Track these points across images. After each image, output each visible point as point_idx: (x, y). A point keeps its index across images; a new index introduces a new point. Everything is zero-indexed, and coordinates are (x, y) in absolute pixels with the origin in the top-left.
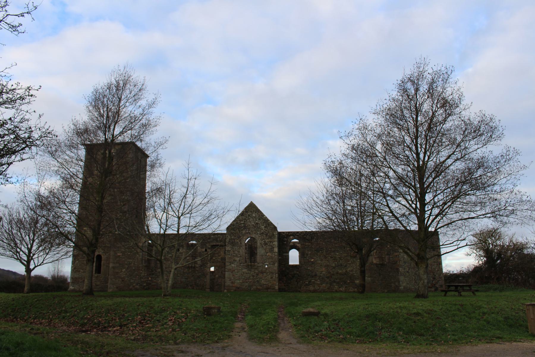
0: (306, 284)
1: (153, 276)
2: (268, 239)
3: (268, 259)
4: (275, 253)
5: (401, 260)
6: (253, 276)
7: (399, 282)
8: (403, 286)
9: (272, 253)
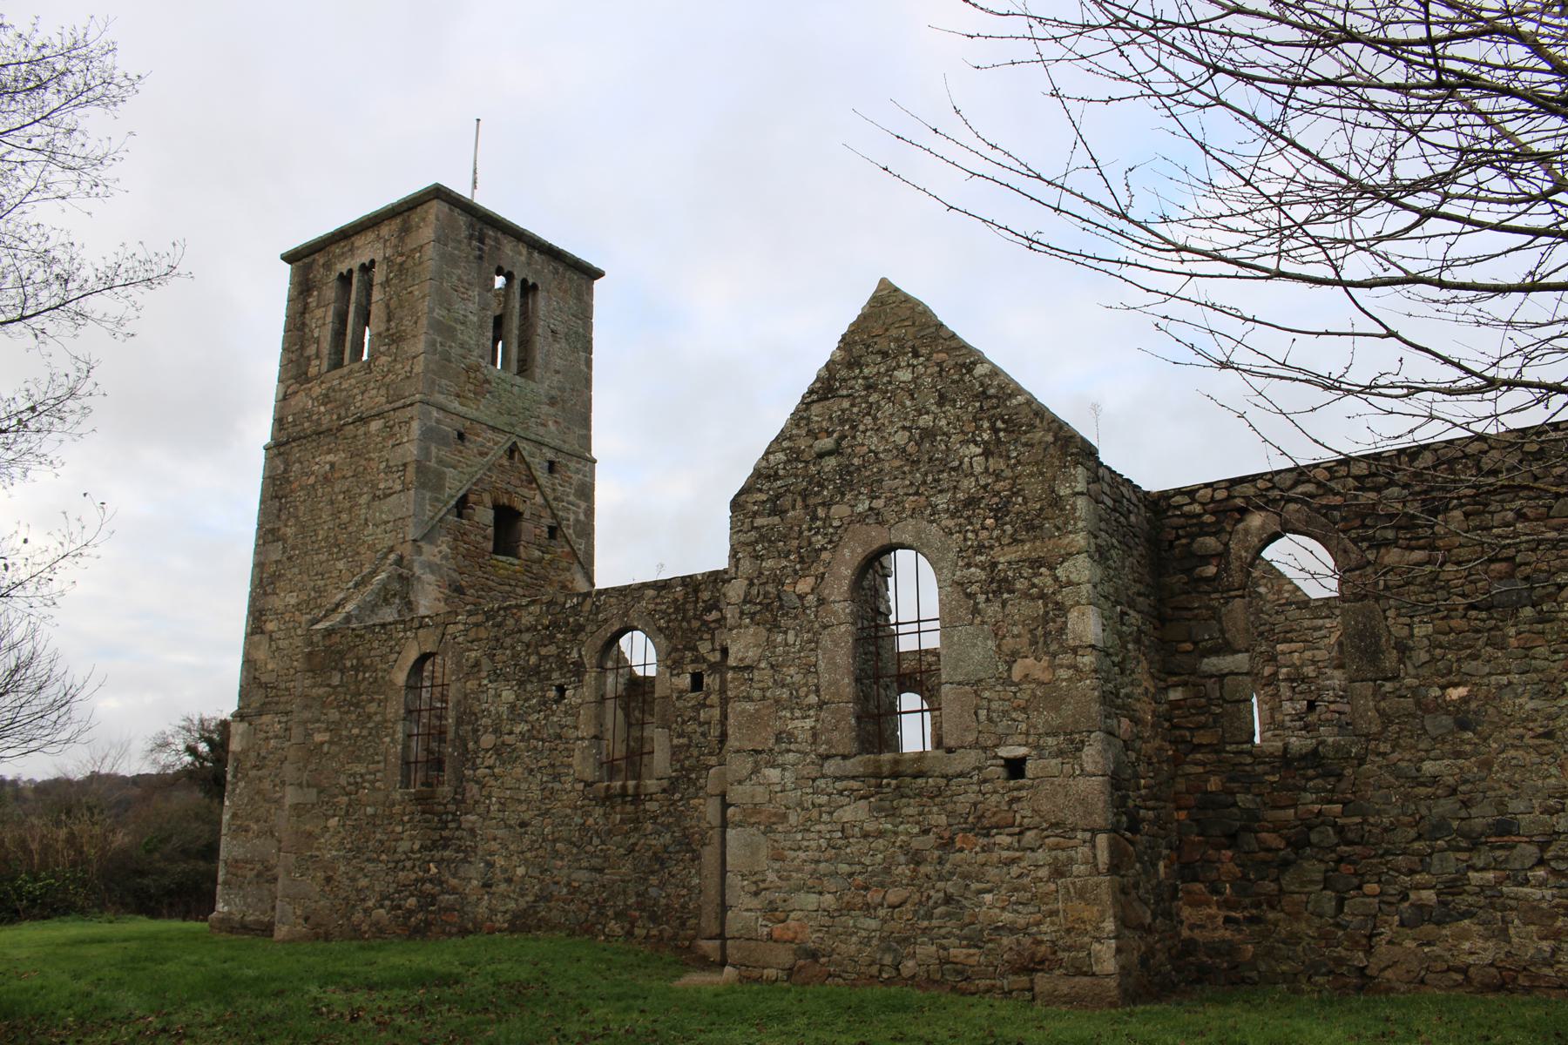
0: (1420, 907)
1: (447, 853)
2: (1015, 541)
3: (1024, 710)
4: (1075, 650)
6: (916, 859)
9: (1054, 655)
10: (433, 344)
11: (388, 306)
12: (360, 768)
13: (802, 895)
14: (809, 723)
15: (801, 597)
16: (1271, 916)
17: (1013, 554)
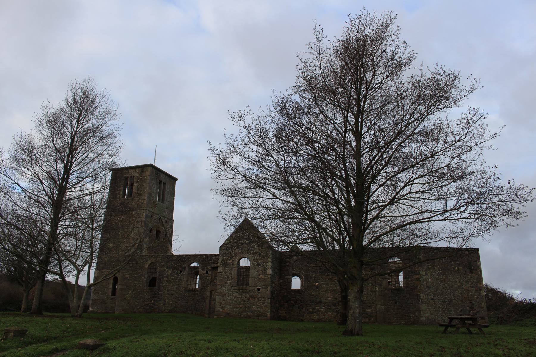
1: (156, 299)
2: (261, 259)
3: (261, 282)
4: (268, 275)
5: (423, 285)
6: (244, 301)
7: (420, 312)
8: (425, 317)
9: (265, 275)
10: (148, 197)
11: (137, 187)
12: (137, 282)
13: (227, 306)
14: (230, 281)
15: (230, 263)
16: (291, 312)
17: (261, 261)
